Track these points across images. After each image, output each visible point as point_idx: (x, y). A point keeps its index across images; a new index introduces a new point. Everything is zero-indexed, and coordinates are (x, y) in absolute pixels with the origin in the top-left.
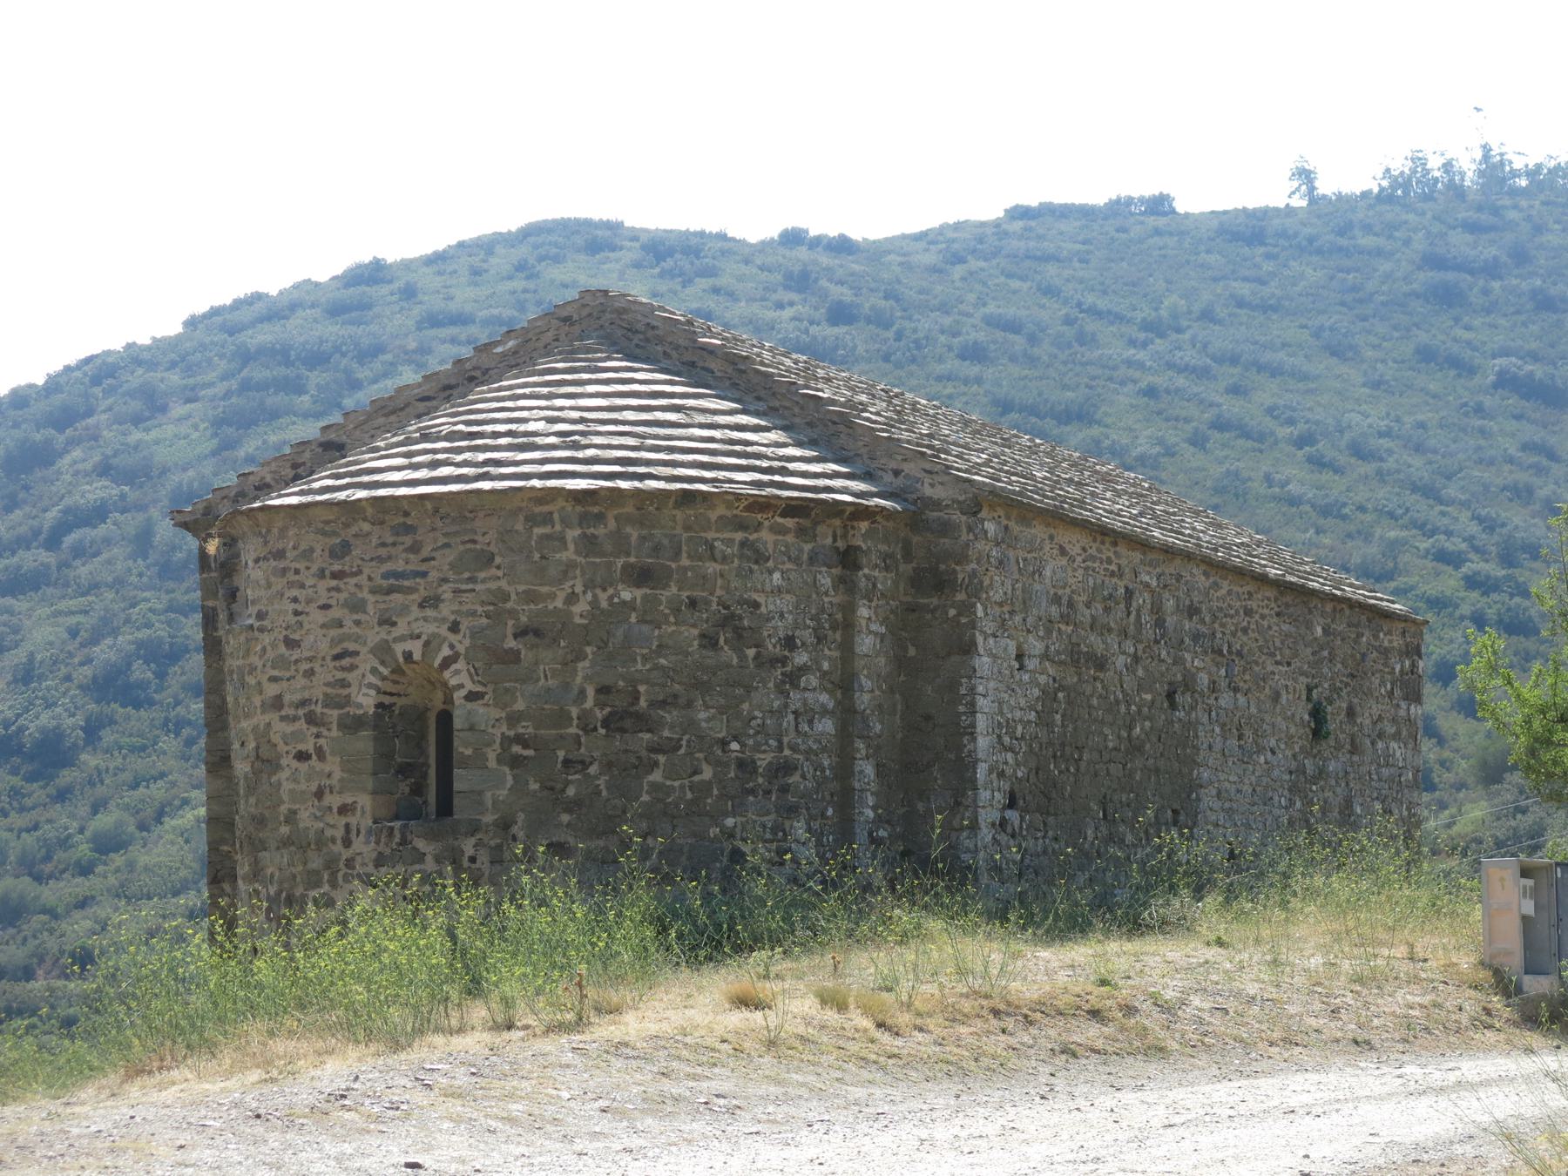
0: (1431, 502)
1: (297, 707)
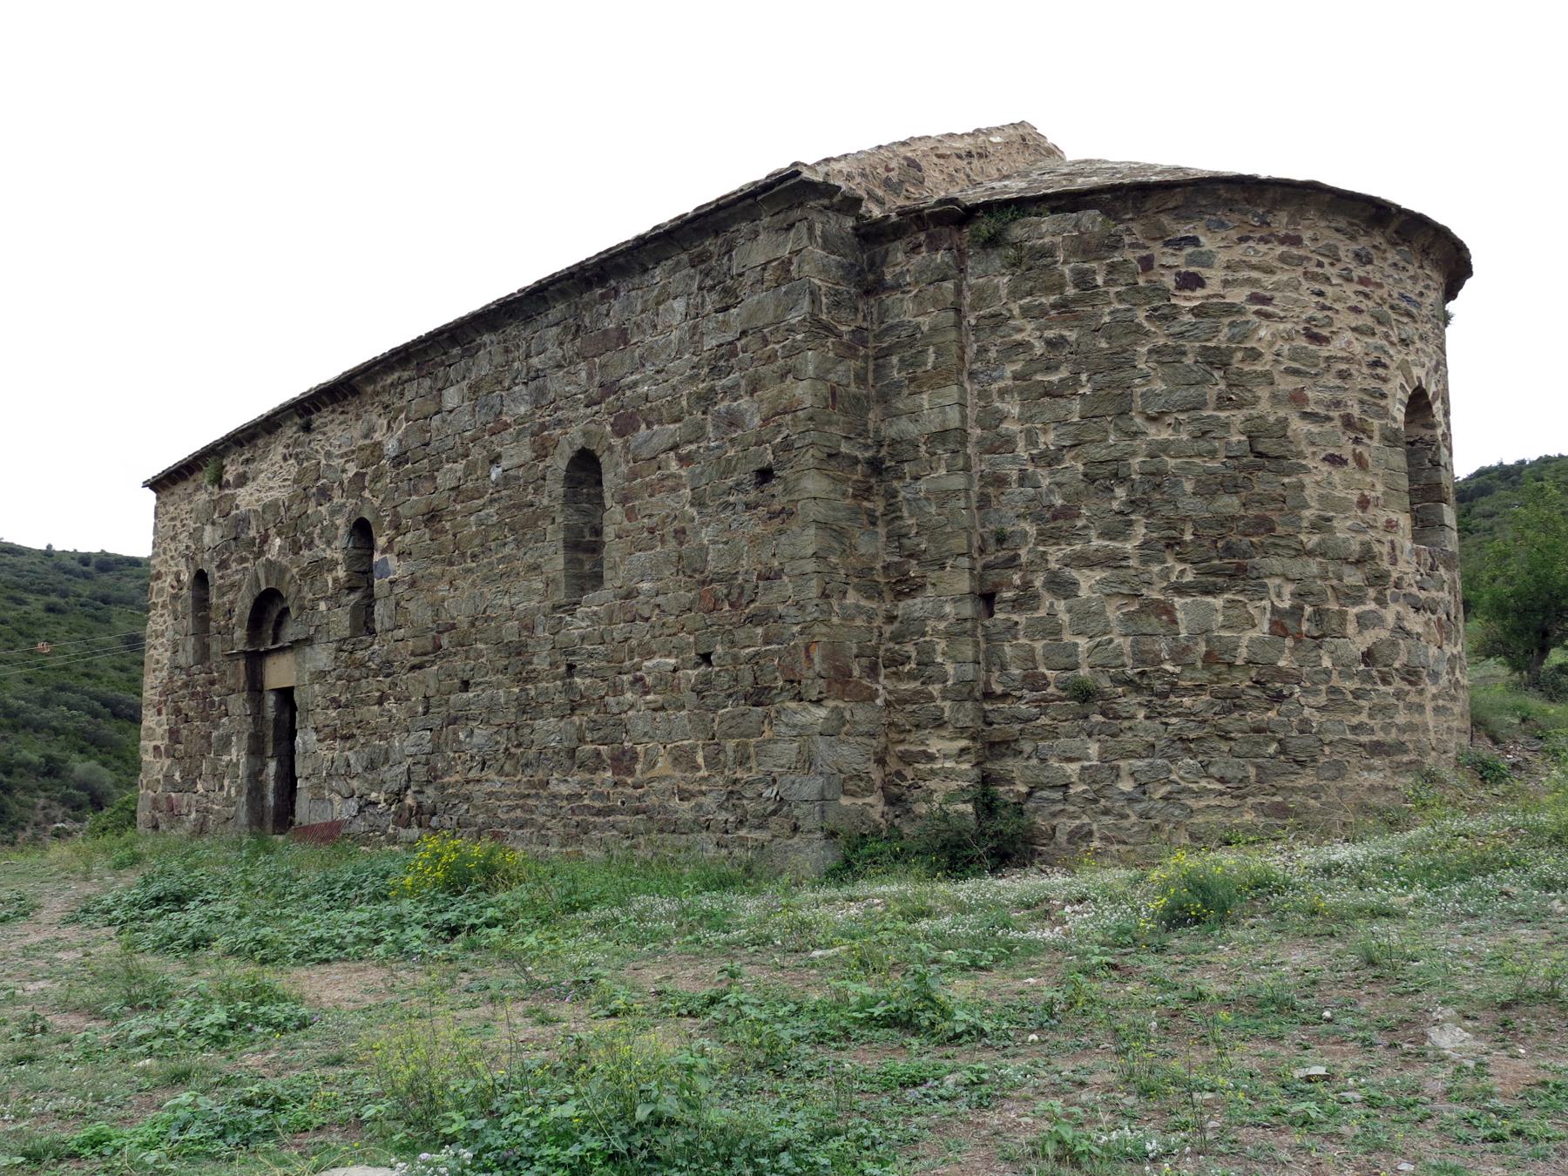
1: (1328, 407)
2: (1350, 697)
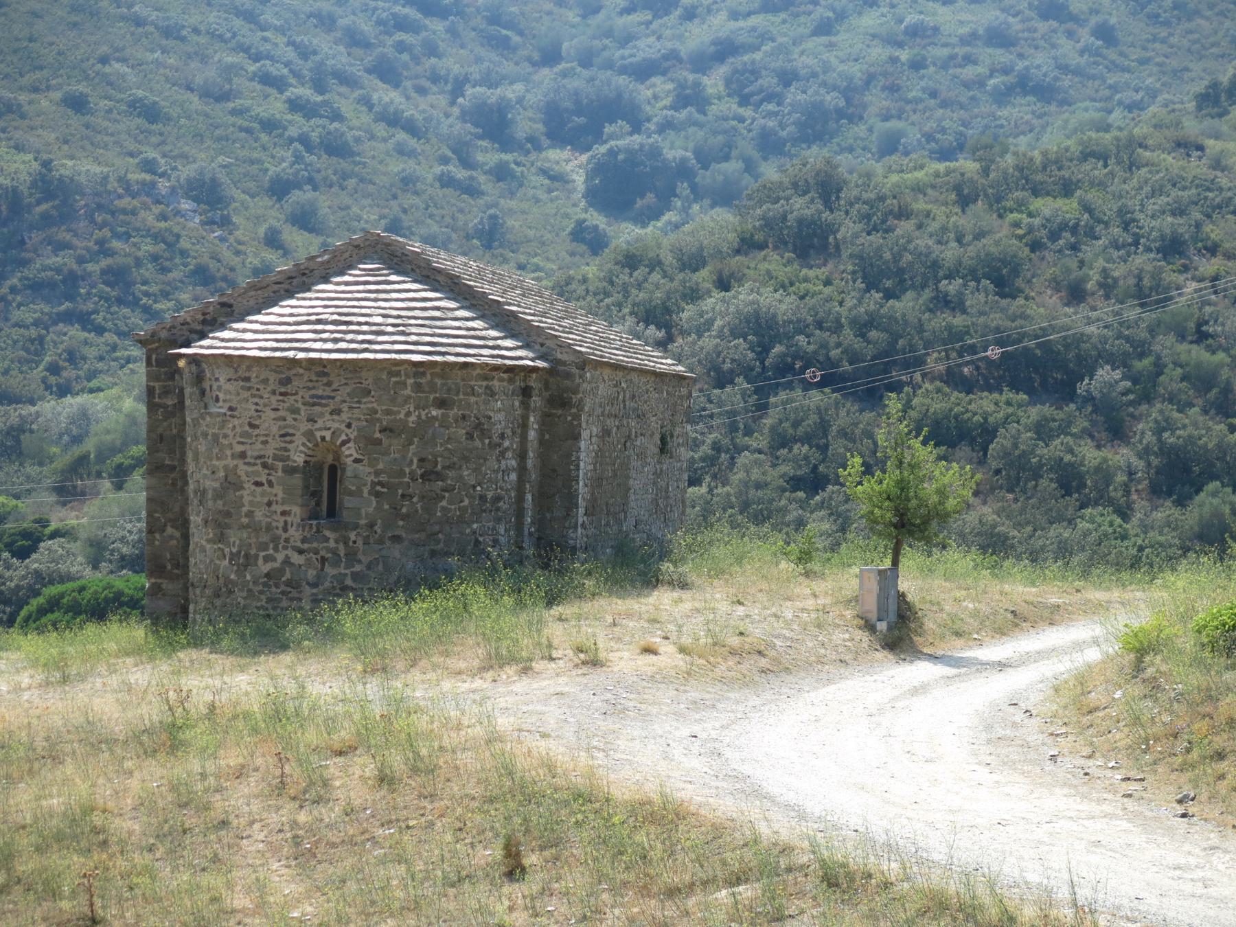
0: (252, 26)
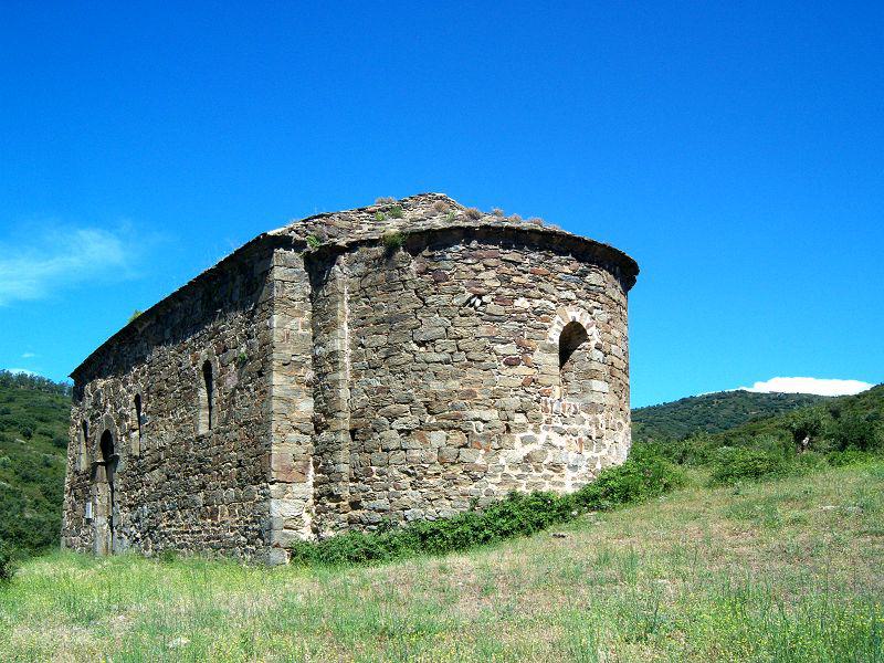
2: (515, 478)
